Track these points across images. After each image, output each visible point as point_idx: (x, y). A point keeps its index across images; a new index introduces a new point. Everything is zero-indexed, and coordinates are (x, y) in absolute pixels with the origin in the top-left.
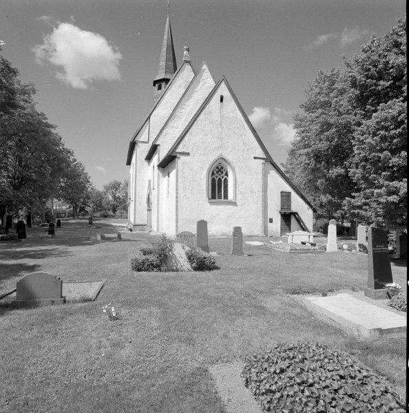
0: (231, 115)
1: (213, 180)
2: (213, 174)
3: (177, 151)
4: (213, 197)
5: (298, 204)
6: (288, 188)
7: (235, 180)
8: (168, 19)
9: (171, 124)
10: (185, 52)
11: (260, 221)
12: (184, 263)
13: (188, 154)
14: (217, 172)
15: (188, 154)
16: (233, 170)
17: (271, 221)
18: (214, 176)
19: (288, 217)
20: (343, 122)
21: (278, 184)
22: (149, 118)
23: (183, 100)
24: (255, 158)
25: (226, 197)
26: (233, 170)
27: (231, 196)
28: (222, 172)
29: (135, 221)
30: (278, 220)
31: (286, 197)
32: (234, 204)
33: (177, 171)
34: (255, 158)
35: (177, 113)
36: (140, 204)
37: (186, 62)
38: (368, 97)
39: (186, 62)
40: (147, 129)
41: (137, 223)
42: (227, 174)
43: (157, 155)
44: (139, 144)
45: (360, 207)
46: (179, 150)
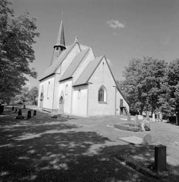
0: (106, 70)
1: (99, 94)
2: (99, 92)
3: (89, 82)
4: (99, 101)
5: (125, 104)
6: (122, 98)
7: (107, 94)
8: (62, 21)
9: (78, 69)
10: (76, 39)
11: (114, 110)
12: (143, 129)
13: (92, 83)
14: (101, 91)
15: (92, 83)
16: (106, 90)
17: (117, 110)
18: (99, 92)
19: (122, 108)
20: (173, 87)
21: (120, 96)
22: (61, 64)
23: (83, 59)
24: (113, 86)
25: (103, 101)
26: (106, 90)
27: (105, 100)
28: (102, 91)
29: (53, 108)
30: (119, 109)
31: (121, 101)
32: (106, 103)
33: (88, 90)
34: (113, 86)
35: (80, 65)
36: (55, 100)
37: (77, 43)
38: (175, 78)
39: (77, 43)
40: (60, 69)
41: (54, 109)
42: (103, 92)
43: (54, 78)
44: (56, 74)
45: (166, 109)
46: (89, 82)
